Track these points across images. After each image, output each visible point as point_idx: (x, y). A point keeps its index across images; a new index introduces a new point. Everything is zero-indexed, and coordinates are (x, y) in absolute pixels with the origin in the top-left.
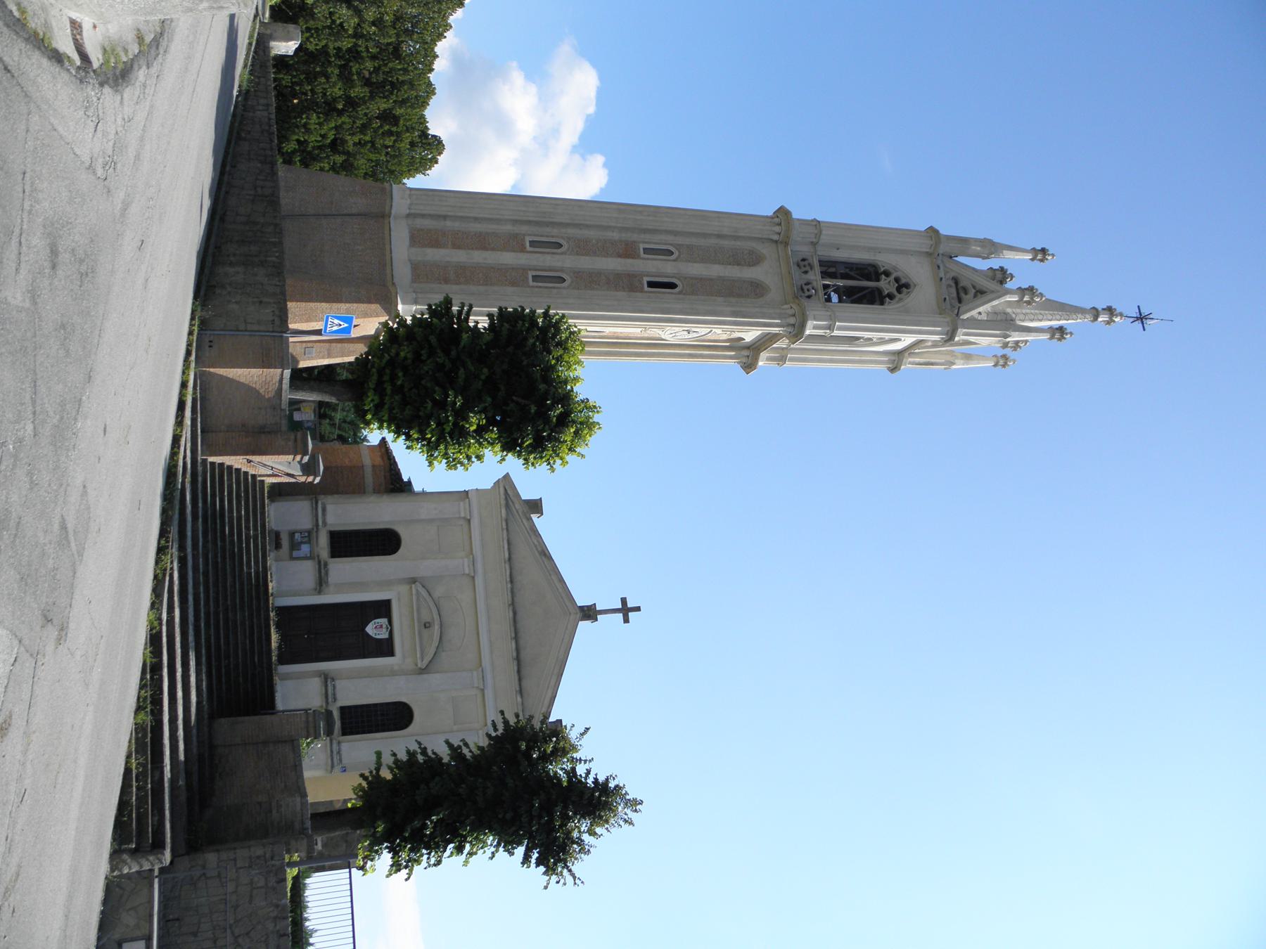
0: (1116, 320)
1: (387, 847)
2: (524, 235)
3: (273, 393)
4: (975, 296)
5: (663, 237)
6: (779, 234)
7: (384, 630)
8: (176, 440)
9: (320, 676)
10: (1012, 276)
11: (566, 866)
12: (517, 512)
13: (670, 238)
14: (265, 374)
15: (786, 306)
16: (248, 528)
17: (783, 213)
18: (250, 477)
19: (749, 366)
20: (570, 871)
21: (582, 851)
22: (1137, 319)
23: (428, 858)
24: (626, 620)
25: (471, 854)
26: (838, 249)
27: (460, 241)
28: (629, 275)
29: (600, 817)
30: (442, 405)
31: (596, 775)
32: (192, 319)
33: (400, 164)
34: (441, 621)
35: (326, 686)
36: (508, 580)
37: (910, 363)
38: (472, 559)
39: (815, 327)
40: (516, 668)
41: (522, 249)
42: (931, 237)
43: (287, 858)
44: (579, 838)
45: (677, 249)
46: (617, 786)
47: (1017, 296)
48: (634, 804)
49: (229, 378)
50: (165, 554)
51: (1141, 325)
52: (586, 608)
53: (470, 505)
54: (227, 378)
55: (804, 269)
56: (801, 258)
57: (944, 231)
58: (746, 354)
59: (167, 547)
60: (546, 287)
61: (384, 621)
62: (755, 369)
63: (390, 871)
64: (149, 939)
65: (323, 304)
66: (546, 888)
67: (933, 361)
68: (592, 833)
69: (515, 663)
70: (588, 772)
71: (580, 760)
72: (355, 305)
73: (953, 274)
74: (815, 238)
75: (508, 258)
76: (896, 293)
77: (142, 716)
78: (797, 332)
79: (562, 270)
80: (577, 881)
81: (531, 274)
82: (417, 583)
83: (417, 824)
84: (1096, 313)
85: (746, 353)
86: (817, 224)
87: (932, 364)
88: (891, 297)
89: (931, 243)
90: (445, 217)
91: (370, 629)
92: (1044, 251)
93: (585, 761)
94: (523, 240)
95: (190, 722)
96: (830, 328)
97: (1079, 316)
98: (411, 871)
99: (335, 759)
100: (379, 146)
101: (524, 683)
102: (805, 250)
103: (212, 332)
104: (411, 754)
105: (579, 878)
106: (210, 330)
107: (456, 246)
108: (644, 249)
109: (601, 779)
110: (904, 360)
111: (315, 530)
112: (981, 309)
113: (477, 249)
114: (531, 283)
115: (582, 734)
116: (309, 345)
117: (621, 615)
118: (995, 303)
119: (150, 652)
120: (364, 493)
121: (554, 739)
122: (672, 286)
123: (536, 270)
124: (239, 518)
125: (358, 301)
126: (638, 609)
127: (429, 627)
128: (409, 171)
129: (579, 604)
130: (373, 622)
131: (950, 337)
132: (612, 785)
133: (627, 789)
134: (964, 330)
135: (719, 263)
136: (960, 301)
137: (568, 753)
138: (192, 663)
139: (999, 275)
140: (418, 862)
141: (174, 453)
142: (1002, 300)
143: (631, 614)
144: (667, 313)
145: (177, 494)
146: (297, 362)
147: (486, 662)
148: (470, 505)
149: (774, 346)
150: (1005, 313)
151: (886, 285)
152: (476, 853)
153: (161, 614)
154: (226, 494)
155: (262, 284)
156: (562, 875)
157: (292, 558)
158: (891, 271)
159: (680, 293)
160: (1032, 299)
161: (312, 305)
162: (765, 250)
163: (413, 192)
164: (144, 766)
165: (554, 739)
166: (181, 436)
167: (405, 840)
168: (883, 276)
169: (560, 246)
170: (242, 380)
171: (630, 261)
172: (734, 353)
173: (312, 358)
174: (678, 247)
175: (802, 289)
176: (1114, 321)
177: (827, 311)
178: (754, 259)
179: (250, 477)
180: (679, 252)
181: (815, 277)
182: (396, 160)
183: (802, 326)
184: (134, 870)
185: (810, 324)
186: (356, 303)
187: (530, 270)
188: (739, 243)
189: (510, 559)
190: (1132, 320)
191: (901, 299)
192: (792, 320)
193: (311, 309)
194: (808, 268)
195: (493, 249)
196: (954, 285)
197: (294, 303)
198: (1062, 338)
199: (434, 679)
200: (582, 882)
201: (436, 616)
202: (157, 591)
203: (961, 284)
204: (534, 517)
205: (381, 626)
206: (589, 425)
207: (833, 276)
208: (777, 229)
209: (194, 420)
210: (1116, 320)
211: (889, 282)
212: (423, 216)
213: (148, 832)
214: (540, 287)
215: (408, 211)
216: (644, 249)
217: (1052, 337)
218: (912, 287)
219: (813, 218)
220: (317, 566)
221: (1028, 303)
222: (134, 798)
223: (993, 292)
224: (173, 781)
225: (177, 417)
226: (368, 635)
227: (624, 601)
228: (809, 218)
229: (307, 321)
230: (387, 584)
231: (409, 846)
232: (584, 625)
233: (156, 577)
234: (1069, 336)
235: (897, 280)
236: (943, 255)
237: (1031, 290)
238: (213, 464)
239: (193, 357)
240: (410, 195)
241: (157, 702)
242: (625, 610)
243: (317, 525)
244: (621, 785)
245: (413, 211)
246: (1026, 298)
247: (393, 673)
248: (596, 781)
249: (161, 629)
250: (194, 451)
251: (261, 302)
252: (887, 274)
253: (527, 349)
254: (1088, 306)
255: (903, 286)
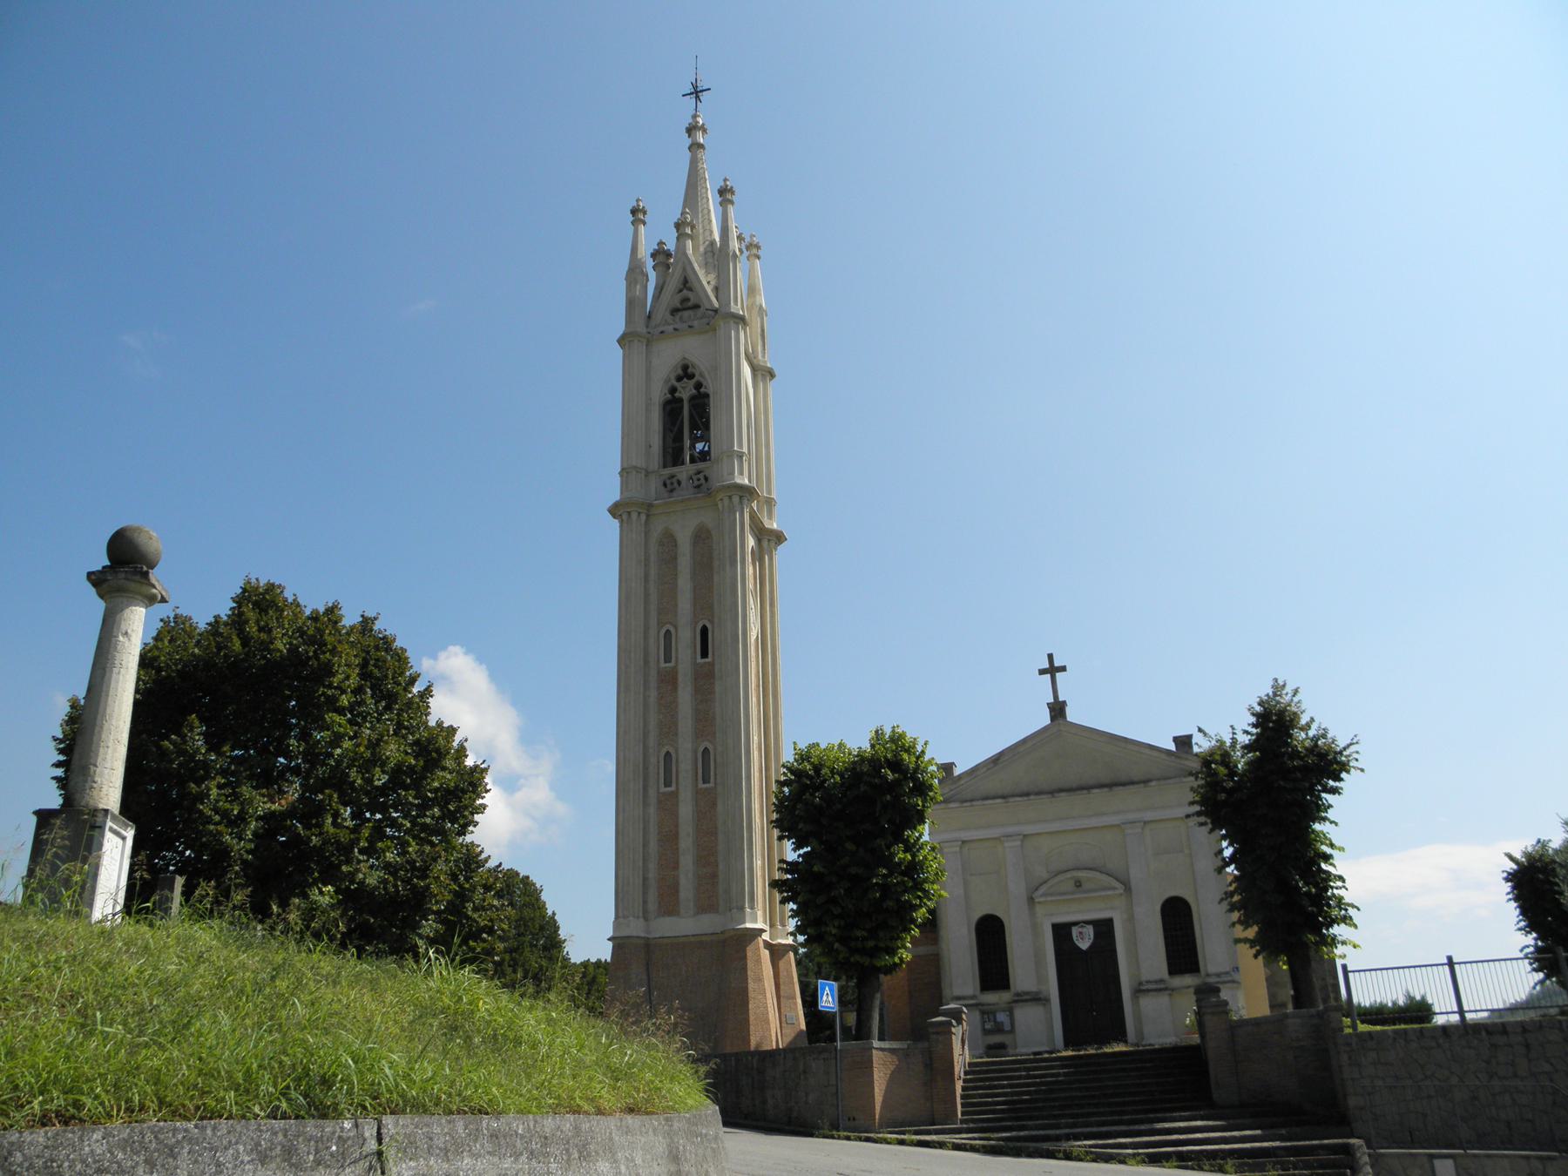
0: (701, 123)
1: (1327, 930)
2: (658, 793)
3: (894, 1057)
4: (690, 289)
5: (652, 641)
6: (639, 513)
7: (1084, 930)
8: (957, 1147)
9: (1138, 997)
10: (661, 243)
11: (1341, 753)
12: (952, 790)
13: (653, 632)
14: (877, 1066)
15: (720, 506)
16: (1020, 1077)
17: (614, 511)
18: (968, 1077)
19: (779, 538)
20: (1345, 749)
21: (1324, 736)
22: (697, 97)
23: (1337, 888)
24: (1063, 669)
25: (1332, 845)
26: (650, 446)
27: (670, 862)
28: (696, 679)
29: (1292, 720)
30: (885, 888)
31: (1249, 725)
32: (832, 1137)
33: (532, 919)
34: (1073, 870)
35: (1148, 991)
36: (1025, 798)
37: (764, 356)
38: (1005, 838)
39: (741, 473)
40: (1121, 788)
41: (675, 794)
42: (630, 341)
43: (1348, 1031)
44: (1312, 740)
45: (662, 627)
46: (1259, 704)
47: (687, 242)
48: (1278, 688)
49: (883, 1100)
50: (1071, 1153)
51: (704, 93)
52: (1053, 714)
53: (947, 842)
54: (882, 1103)
55: (676, 485)
56: (663, 488)
57: (620, 327)
58: (767, 543)
59: (1065, 1151)
60: (715, 768)
61: (1075, 931)
62: (782, 532)
63: (1350, 925)
64: (1432, 1157)
65: (750, 1006)
66: (1362, 770)
67: (759, 330)
68: (1308, 726)
69: (1115, 789)
70: (1246, 732)
71: (1232, 739)
72: (749, 973)
73: (668, 314)
74: (641, 473)
75: (686, 810)
76: (694, 381)
77: (1228, 1167)
78: (747, 493)
79: (695, 752)
80: (1354, 741)
81: (701, 785)
82: (1034, 896)
83: (1305, 902)
84: (695, 147)
85: (765, 543)
86: (625, 472)
87: (763, 331)
88: (699, 386)
89: (636, 341)
90: (645, 879)
91: (1084, 945)
92: (634, 212)
93: (1234, 733)
94: (664, 794)
95: (1222, 1125)
96: (740, 456)
97: (700, 165)
98: (1349, 905)
99: (1226, 979)
100: (516, 943)
101: (1136, 779)
102: (655, 484)
103: (840, 1117)
104: (1232, 908)
105: (1352, 740)
106: (838, 1119)
107: (676, 867)
108: (666, 662)
109: (1253, 720)
110: (762, 364)
111: (980, 1007)
112: (705, 283)
113: (677, 844)
114: (711, 785)
115: (1205, 734)
116: (784, 1019)
117: (1058, 675)
118: (696, 266)
119: (1167, 1162)
120: (938, 955)
121: (1213, 766)
122: (704, 631)
123: (697, 780)
124: (1011, 1086)
125: (744, 969)
126: (1050, 657)
127: (1079, 882)
128: (539, 908)
129: (1048, 721)
130: (1076, 942)
131: (741, 320)
132: (1258, 709)
133: (1263, 695)
134: (732, 304)
135: (676, 579)
136: (697, 307)
137: (1226, 751)
138: (1167, 1125)
139: (661, 258)
140: (1340, 899)
141: (973, 1149)
142: (693, 259)
143: (1056, 665)
144: (735, 637)
145: (1011, 1144)
146: (802, 1031)
147: (1115, 820)
148: (947, 842)
149: (755, 509)
150: (705, 253)
151: (686, 392)
152: (1330, 840)
153: (1129, 1154)
154: (990, 1100)
155: (785, 1071)
156: (1349, 756)
157: (1012, 1031)
158: (670, 384)
159: (712, 622)
160: (689, 224)
161: (752, 1018)
162: (658, 528)
163: (621, 914)
164: (1275, 1163)
165: (1213, 766)
166: (954, 1143)
167: (1321, 912)
168: (677, 395)
169: (668, 754)
170: (884, 1087)
171: (680, 679)
172: (766, 557)
173: (797, 1016)
174: (660, 624)
175: (698, 487)
176: (703, 124)
177: (722, 460)
178: (669, 540)
179: (968, 1077)
180: (667, 623)
181: (685, 471)
182: (529, 924)
183: (741, 487)
184: (1371, 1171)
185: (738, 480)
186: (747, 971)
187: (697, 786)
188: (653, 558)
189: (1003, 797)
190: (699, 103)
191: (702, 375)
192: (736, 499)
193: (755, 1019)
194: (674, 480)
195: (677, 826)
196: (680, 314)
197: (751, 1038)
198: (731, 191)
199: (1136, 875)
200: (1355, 736)
201: (1069, 875)
202: (1108, 1159)
203: (679, 306)
204: (957, 772)
205: (1081, 933)
206: (897, 738)
207: (681, 450)
208: (634, 516)
209: (937, 1132)
210: (701, 123)
211: (683, 387)
212: (645, 902)
213: (1335, 1159)
214: (715, 775)
215: (642, 920)
216: (666, 662)
217: (732, 202)
218: (686, 361)
219: (618, 475)
220: (1021, 1004)
221: (693, 227)
222: (1305, 1172)
223: (684, 270)
224: (1282, 1139)
225: (935, 1147)
226: (1090, 947)
227: (1042, 672)
228: (618, 478)
229: (768, 1022)
230: (1035, 929)
231: (1325, 908)
232: (1072, 715)
233: (1094, 1161)
234: (728, 183)
235: (679, 379)
236: (647, 327)
237: (678, 226)
238: (963, 1114)
239: (872, 1135)
240: (624, 917)
241: (1213, 1155)
242: (1052, 670)
243: (977, 1005)
244: (1258, 699)
245: (641, 914)
246: (688, 231)
247: (1131, 919)
248: (1254, 726)
249: (1145, 1154)
250: (959, 1131)
251: (805, 1072)
252: (673, 390)
253: (824, 805)
254: (689, 154)
255: (686, 372)
